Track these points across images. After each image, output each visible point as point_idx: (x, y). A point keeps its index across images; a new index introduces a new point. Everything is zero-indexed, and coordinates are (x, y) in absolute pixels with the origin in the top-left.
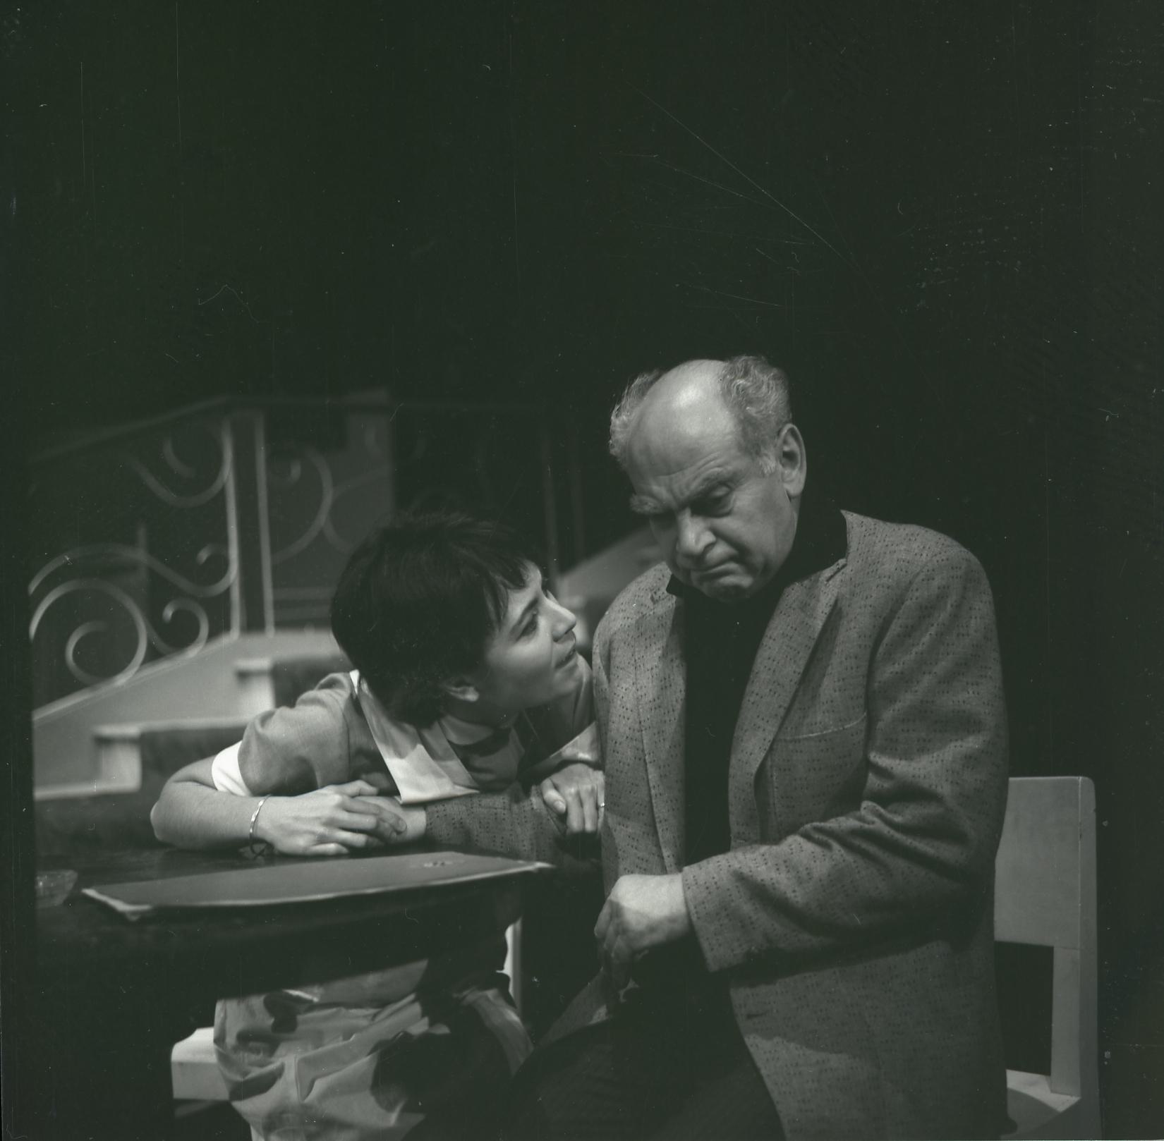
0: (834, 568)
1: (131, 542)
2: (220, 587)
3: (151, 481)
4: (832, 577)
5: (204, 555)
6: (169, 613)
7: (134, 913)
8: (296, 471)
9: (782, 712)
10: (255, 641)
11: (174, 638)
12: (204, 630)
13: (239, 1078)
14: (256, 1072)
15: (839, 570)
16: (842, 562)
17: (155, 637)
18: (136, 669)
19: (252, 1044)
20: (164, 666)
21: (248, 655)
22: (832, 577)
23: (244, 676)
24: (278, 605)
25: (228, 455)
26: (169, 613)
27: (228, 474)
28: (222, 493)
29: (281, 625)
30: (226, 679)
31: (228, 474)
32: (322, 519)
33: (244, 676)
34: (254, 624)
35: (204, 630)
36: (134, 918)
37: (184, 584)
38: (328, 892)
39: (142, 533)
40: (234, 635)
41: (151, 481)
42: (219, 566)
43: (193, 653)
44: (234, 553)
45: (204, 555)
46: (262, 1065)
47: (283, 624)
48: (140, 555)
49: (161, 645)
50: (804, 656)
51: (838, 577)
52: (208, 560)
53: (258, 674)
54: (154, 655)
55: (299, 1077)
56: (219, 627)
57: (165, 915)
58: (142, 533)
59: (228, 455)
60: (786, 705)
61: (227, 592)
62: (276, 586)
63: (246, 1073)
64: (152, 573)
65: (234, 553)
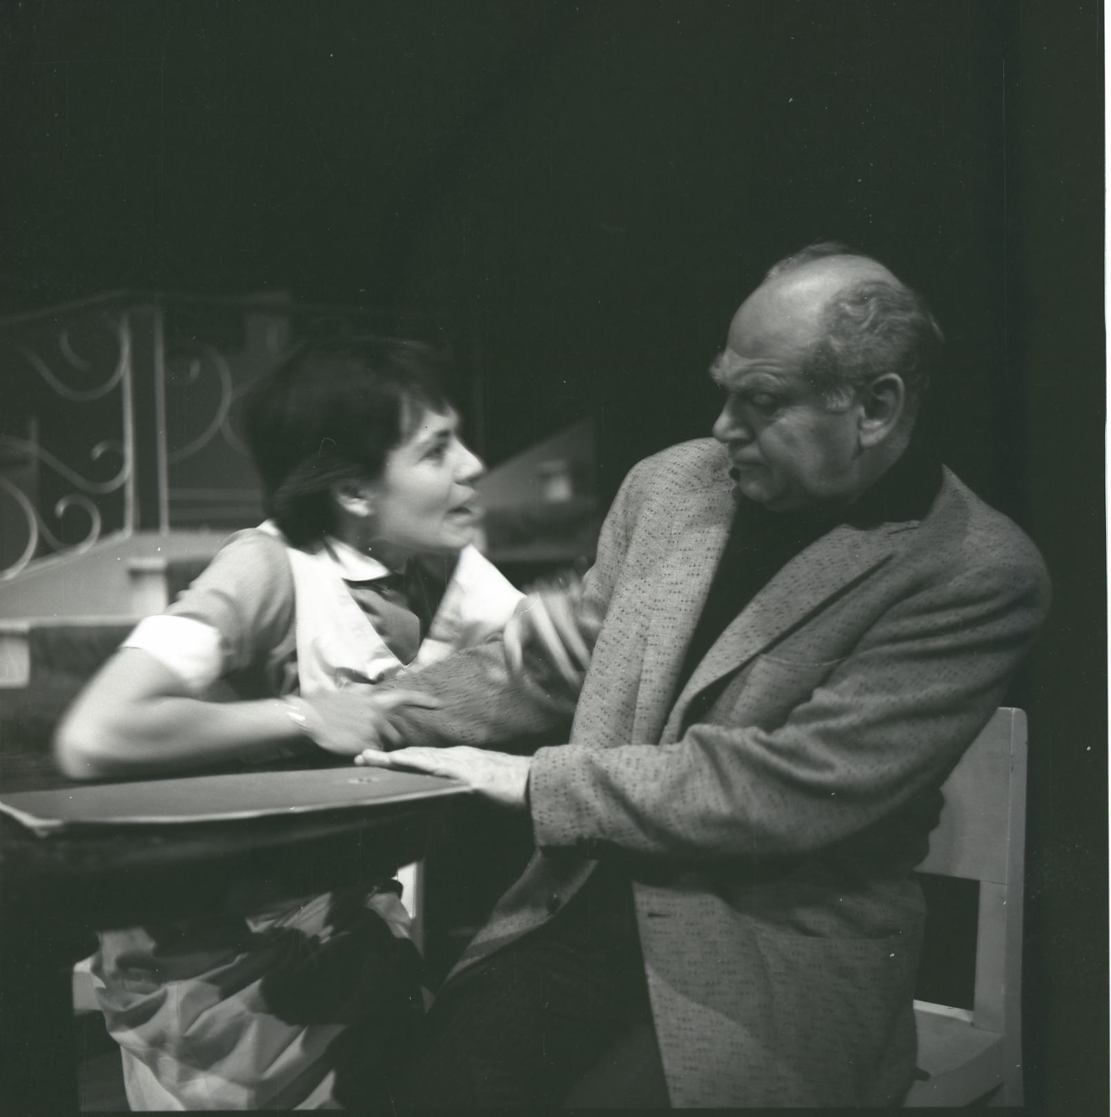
0: (904, 525)
1: (24, 436)
2: (115, 484)
3: (47, 375)
4: (896, 532)
5: (98, 451)
6: (61, 508)
7: (43, 828)
8: (195, 369)
9: (777, 633)
10: (148, 540)
11: (63, 535)
12: (97, 528)
13: (121, 1009)
14: (140, 999)
15: (907, 529)
16: (915, 523)
17: (47, 533)
18: (25, 564)
19: (133, 970)
20: (54, 562)
21: (141, 553)
22: (896, 532)
23: (136, 575)
24: (173, 504)
25: (126, 350)
26: (61, 508)
27: (125, 371)
28: (119, 388)
29: (176, 525)
30: (119, 578)
31: (125, 371)
32: (221, 419)
33: (136, 575)
34: (148, 523)
35: (97, 528)
36: (43, 834)
37: (79, 481)
38: (271, 806)
39: (33, 426)
40: (127, 533)
41: (47, 375)
42: (114, 462)
43: (85, 549)
44: (129, 450)
45: (98, 451)
46: (146, 992)
47: (178, 524)
48: (31, 448)
49: (52, 540)
50: (828, 592)
51: (903, 535)
52: (103, 455)
53: (152, 573)
54: (45, 551)
55: (183, 1007)
56: (112, 524)
57: (79, 834)
58: (33, 426)
59: (126, 350)
60: (784, 629)
61: (121, 490)
62: (172, 485)
63: (127, 1003)
64: (44, 467)
65: (129, 450)
